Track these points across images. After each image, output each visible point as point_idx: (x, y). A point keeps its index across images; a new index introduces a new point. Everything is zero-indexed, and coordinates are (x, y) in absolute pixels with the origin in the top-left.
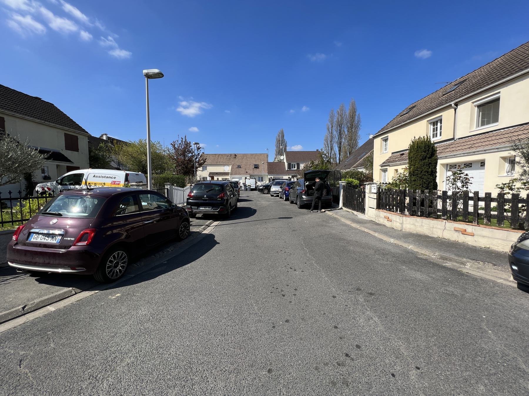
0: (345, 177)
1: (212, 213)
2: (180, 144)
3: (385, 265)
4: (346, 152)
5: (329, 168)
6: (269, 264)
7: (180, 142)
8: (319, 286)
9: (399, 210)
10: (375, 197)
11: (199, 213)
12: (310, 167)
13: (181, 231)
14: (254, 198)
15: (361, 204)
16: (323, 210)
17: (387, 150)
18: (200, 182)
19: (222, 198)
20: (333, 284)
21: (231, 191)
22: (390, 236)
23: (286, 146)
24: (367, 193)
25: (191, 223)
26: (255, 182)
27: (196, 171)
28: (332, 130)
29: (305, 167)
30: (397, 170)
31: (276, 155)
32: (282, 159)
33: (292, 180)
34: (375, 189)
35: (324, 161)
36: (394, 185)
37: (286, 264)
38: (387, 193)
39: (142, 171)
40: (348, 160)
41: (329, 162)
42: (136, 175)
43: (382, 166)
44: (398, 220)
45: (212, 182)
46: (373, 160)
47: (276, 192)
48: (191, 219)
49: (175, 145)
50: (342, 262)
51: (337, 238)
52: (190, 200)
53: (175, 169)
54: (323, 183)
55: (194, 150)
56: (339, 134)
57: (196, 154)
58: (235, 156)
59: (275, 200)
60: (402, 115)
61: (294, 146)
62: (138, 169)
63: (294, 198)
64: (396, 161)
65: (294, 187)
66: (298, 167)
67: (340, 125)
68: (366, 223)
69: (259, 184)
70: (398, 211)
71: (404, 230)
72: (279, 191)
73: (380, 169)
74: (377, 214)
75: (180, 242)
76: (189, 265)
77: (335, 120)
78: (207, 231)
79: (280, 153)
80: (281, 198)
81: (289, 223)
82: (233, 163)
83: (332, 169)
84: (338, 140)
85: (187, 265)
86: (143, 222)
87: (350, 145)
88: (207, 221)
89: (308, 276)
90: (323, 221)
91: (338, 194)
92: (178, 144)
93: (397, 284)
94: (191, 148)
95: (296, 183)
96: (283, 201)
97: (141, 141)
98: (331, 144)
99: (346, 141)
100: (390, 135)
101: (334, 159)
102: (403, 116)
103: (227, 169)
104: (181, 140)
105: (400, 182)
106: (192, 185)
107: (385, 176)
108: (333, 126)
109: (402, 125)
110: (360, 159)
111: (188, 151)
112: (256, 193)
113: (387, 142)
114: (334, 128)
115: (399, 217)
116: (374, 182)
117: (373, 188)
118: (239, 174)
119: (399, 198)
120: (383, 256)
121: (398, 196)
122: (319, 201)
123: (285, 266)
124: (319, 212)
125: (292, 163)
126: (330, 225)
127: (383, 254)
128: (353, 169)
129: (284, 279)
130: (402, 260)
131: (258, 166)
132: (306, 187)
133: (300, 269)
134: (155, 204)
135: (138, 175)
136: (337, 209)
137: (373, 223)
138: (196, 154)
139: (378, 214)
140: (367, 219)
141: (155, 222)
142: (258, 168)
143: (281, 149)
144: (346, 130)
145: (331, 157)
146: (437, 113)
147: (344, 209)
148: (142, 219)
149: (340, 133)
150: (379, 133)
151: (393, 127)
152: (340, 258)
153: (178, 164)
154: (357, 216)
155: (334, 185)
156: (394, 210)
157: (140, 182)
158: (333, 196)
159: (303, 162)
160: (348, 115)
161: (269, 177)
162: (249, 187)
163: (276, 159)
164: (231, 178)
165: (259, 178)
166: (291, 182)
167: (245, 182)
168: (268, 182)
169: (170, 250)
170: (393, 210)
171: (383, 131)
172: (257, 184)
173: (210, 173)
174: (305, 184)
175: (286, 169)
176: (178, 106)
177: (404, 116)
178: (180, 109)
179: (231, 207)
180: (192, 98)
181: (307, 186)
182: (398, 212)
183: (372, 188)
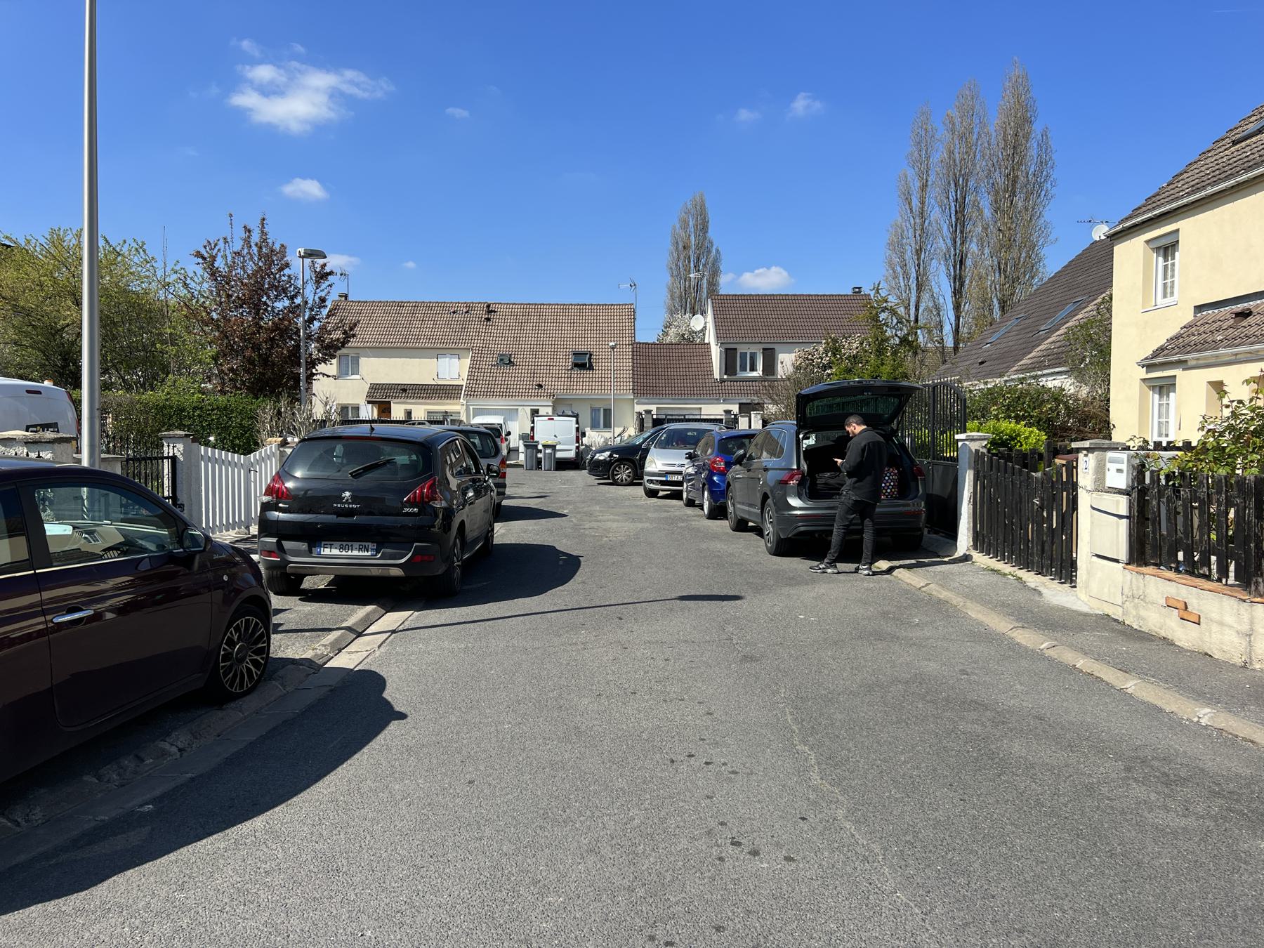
0: (984, 414)
1: (375, 572)
2: (238, 254)
3: (1175, 834)
4: (985, 301)
5: (910, 372)
6: (632, 819)
7: (238, 245)
8: (865, 935)
9: (1232, 568)
10: (1124, 511)
11: (321, 571)
12: (825, 367)
13: (227, 657)
14: (569, 503)
15: (1056, 540)
16: (883, 565)
17: (1172, 294)
18: (328, 431)
19: (423, 504)
20: (932, 924)
21: (467, 471)
22: (1194, 691)
23: (715, 272)
24: (1085, 488)
25: (275, 620)
26: (577, 429)
27: (310, 377)
28: (923, 203)
29: (798, 368)
30: (1219, 387)
31: (672, 312)
32: (698, 328)
33: (743, 424)
34: (1119, 471)
35: (887, 339)
36: (1211, 453)
37: (712, 823)
38: (1176, 490)
39: (61, 375)
40: (996, 336)
41: (910, 343)
42: (28, 392)
43: (1150, 368)
44: (1229, 619)
45: (382, 430)
46: (1110, 337)
47: (670, 478)
48: (276, 601)
49: (214, 258)
50: (974, 817)
51: (947, 700)
52: (277, 513)
53: (210, 369)
54: (881, 439)
55: (299, 283)
56: (954, 219)
57: (310, 302)
58: (490, 312)
59: (665, 514)
60: (1238, 136)
61: (753, 272)
62: (42, 366)
63: (750, 505)
64: (1216, 345)
65: (751, 458)
66: (770, 367)
67: (959, 181)
68: (1082, 629)
69: (594, 438)
70: (1232, 574)
71: (1257, 666)
72: (680, 473)
73: (1144, 380)
74: (1131, 588)
75: (221, 709)
76: (257, 823)
77: (939, 155)
78: (353, 656)
79: (689, 302)
80: (690, 503)
81: (727, 621)
82: (477, 343)
83: (925, 376)
84: (950, 244)
85: (248, 823)
86: (48, 618)
87: (1005, 271)
88: (353, 611)
89: (816, 884)
90: (884, 615)
91: (949, 489)
92: (228, 252)
93: (1232, 929)
94: (287, 271)
95: (758, 440)
96: (699, 519)
97: (56, 239)
98: (919, 265)
99: (987, 251)
100: (1187, 227)
101: (930, 332)
102: (1243, 144)
103: (454, 370)
104: (244, 235)
105: (1236, 440)
106: (289, 439)
107: (1164, 411)
108: (929, 183)
109: (1239, 185)
110: (1051, 331)
111: (272, 286)
112: (582, 478)
113: (1173, 258)
114: (935, 192)
115: (1233, 602)
116: (1118, 436)
117: (1112, 467)
118: (505, 395)
119: (1232, 515)
120: (1166, 791)
121: (1229, 504)
122: (862, 524)
123: (709, 833)
124: (866, 572)
125: (741, 349)
126: (915, 634)
127: (1164, 779)
128: (1019, 379)
129: (701, 897)
130: (1252, 811)
131: (590, 359)
132: (806, 459)
133: (779, 845)
134: (111, 531)
135: (39, 393)
136: (946, 559)
137: (1113, 630)
138: (310, 302)
139: (1138, 588)
140: (1085, 609)
141: (109, 616)
142: (591, 368)
143: (692, 283)
144: (986, 203)
145: (916, 320)
146: (1163, 223)
147: (977, 556)
148: (42, 603)
149: (960, 215)
150: (1136, 216)
151: (1198, 190)
152: (966, 797)
153: (229, 344)
154: (1040, 594)
155: (931, 450)
156: (1210, 570)
157: (46, 427)
158: (930, 500)
159: (789, 345)
160: (994, 134)
161: (640, 408)
162: (549, 451)
163: (672, 331)
164: (467, 410)
165: (595, 411)
166: (732, 433)
167: (532, 429)
168: (632, 431)
169: (174, 749)
170: (1205, 570)
171: (1154, 208)
172: (585, 440)
173: (375, 388)
174: (798, 443)
175: (717, 375)
176: (235, 83)
177: (1248, 142)
178: (247, 100)
179: (465, 545)
180: (300, 49)
181: (810, 453)
182: (1231, 580)
183: (1109, 465)
